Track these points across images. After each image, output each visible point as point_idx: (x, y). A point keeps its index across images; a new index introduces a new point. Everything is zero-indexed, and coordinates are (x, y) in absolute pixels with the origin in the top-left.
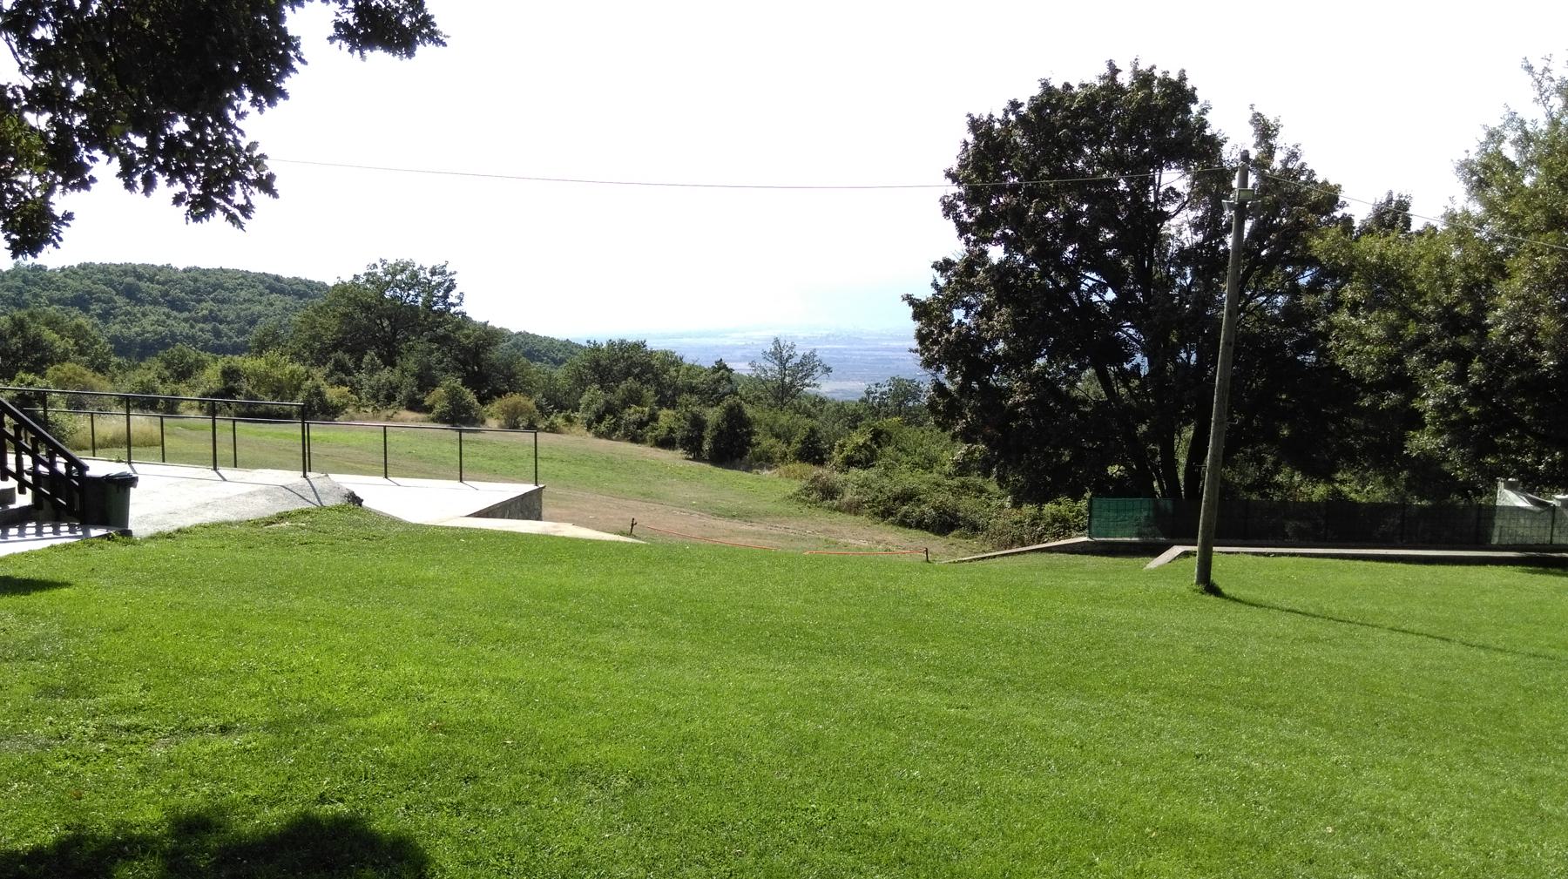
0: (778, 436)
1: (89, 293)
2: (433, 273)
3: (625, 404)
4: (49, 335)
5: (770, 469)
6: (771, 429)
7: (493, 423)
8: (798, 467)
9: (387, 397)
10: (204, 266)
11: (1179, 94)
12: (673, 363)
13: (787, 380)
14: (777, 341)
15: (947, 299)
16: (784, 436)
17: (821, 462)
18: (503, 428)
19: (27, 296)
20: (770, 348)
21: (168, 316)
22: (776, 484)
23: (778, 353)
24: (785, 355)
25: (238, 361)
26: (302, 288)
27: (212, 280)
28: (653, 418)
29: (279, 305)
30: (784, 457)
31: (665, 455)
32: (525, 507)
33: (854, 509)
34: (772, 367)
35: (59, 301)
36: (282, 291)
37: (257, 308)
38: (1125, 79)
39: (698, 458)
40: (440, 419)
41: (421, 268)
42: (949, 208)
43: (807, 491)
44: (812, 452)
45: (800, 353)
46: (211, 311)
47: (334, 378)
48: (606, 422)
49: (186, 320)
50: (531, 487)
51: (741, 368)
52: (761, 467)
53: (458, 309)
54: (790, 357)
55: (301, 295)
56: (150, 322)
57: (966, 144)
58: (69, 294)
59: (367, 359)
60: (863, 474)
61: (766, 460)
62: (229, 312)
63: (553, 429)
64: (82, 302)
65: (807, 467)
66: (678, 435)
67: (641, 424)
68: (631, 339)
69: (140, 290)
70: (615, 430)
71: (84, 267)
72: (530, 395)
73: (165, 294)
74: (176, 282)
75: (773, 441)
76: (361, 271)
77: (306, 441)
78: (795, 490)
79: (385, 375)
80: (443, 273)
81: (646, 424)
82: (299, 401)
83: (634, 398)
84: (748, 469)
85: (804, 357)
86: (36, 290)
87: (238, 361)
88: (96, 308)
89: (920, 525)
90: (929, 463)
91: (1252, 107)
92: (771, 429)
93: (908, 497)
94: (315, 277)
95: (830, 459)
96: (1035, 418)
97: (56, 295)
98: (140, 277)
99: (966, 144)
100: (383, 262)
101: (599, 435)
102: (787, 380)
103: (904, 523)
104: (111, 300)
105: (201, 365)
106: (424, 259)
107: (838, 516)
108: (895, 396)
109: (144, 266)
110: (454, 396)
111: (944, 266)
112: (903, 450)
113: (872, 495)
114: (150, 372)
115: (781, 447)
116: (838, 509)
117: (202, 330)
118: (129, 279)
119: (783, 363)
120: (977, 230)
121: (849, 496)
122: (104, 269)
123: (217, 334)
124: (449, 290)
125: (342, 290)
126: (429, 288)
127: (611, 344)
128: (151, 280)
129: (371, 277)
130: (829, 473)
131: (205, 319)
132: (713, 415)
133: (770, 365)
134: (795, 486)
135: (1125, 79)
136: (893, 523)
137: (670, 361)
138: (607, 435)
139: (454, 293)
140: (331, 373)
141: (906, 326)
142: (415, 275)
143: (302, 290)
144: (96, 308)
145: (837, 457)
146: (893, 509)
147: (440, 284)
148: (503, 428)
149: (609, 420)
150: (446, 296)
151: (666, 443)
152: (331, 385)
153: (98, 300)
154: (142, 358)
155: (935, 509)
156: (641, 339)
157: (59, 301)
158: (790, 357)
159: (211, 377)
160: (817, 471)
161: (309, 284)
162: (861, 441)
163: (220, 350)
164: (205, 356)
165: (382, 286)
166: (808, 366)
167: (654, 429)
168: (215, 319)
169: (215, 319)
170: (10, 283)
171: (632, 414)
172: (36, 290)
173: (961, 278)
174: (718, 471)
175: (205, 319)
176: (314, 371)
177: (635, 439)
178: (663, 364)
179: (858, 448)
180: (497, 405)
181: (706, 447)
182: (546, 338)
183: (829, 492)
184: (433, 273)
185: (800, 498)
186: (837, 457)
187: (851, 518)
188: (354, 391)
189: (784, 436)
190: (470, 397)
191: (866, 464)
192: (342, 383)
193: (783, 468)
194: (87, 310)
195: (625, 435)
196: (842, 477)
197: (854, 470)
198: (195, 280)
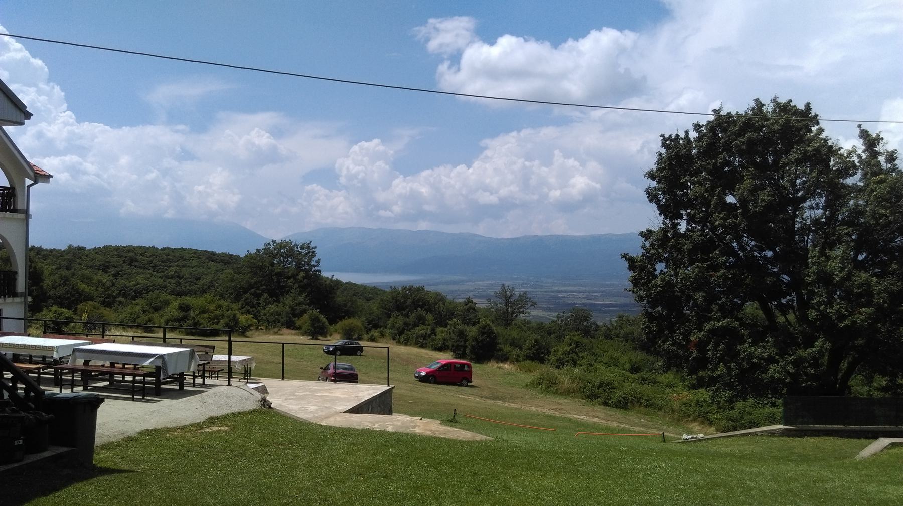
3: (416, 325)
4: (82, 286)
11: (807, 117)
12: (440, 300)
15: (651, 258)
16: (514, 344)
21: (152, 275)
25: (188, 300)
27: (177, 254)
28: (433, 332)
29: (213, 269)
32: (380, 405)
33: (568, 393)
37: (201, 270)
38: (769, 108)
41: (296, 245)
42: (652, 196)
44: (538, 355)
45: (517, 294)
46: (176, 272)
47: (244, 310)
48: (788, 436)
49: (161, 278)
50: (385, 388)
51: (481, 304)
53: (316, 268)
54: (511, 296)
55: (226, 263)
56: (141, 279)
57: (660, 155)
61: (504, 359)
62: (186, 272)
63: (372, 339)
66: (450, 343)
67: (425, 337)
71: (105, 247)
77: (230, 342)
79: (272, 308)
81: (429, 336)
83: (421, 321)
87: (188, 300)
88: (113, 271)
90: (615, 362)
91: (860, 126)
94: (234, 252)
98: (136, 254)
99: (660, 155)
105: (167, 303)
109: (139, 247)
111: (647, 235)
114: (137, 306)
117: (169, 283)
118: (131, 254)
120: (669, 210)
122: (117, 248)
123: (179, 284)
125: (250, 258)
127: (404, 289)
129: (267, 250)
131: (172, 277)
132: (472, 332)
134: (529, 378)
135: (769, 108)
137: (440, 299)
139: (314, 259)
140: (242, 307)
141: (624, 276)
142: (292, 249)
143: (227, 260)
146: (597, 394)
150: (310, 261)
152: (242, 314)
154: (134, 298)
156: (421, 285)
157: (91, 267)
158: (511, 296)
159: (172, 310)
162: (569, 348)
163: (179, 294)
164: (169, 297)
166: (524, 301)
168: (179, 277)
169: (179, 277)
170: (66, 257)
173: (661, 243)
175: (172, 277)
176: (233, 306)
180: (341, 324)
182: (362, 286)
184: (302, 248)
186: (553, 358)
188: (255, 317)
190: (323, 318)
192: (248, 312)
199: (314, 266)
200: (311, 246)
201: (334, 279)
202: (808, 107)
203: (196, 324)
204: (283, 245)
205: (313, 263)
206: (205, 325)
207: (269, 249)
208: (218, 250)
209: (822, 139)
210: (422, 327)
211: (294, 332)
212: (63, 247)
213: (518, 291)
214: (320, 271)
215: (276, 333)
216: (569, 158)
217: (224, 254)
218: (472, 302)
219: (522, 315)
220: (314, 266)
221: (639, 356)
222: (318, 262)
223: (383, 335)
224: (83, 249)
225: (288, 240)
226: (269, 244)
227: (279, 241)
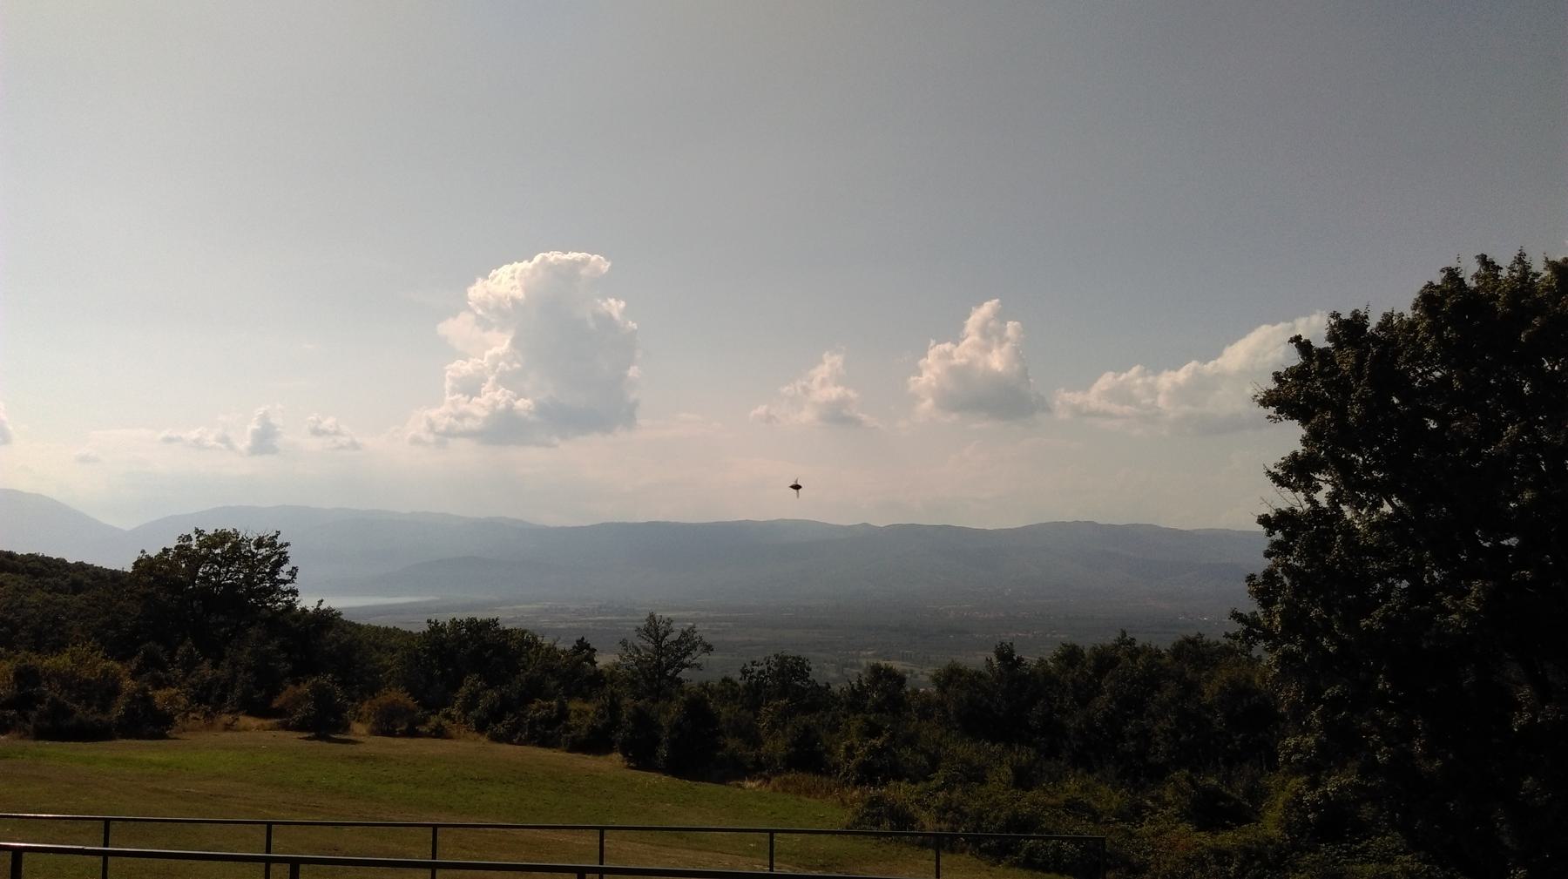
3: (526, 699)
7: (359, 729)
9: (210, 700)
14: (652, 616)
23: (654, 629)
24: (661, 633)
26: (38, 565)
33: (940, 844)
36: (15, 570)
59: (182, 650)
67: (549, 722)
76: (172, 544)
80: (272, 544)
82: (118, 709)
85: (684, 634)
93: (1023, 825)
96: (672, 678)
100: (199, 532)
101: (496, 738)
124: (279, 564)
126: (250, 561)
129: (182, 550)
130: (900, 792)
132: (669, 714)
133: (644, 643)
138: (506, 739)
139: (286, 568)
142: (236, 546)
147: (269, 557)
149: (509, 719)
150: (274, 572)
151: (595, 744)
158: (667, 633)
161: (47, 562)
166: (688, 643)
177: (545, 742)
183: (902, 821)
199: (285, 582)
200: (279, 541)
201: (322, 607)
204: (221, 538)
205: (282, 576)
207: (188, 548)
208: (21, 549)
209: (1381, 327)
211: (268, 722)
214: (295, 593)
215: (228, 727)
216: (196, 441)
217: (32, 558)
218: (587, 647)
219: (685, 670)
220: (285, 582)
222: (293, 573)
224: (63, 562)
225: (250, 529)
226: (189, 538)
227: (210, 532)
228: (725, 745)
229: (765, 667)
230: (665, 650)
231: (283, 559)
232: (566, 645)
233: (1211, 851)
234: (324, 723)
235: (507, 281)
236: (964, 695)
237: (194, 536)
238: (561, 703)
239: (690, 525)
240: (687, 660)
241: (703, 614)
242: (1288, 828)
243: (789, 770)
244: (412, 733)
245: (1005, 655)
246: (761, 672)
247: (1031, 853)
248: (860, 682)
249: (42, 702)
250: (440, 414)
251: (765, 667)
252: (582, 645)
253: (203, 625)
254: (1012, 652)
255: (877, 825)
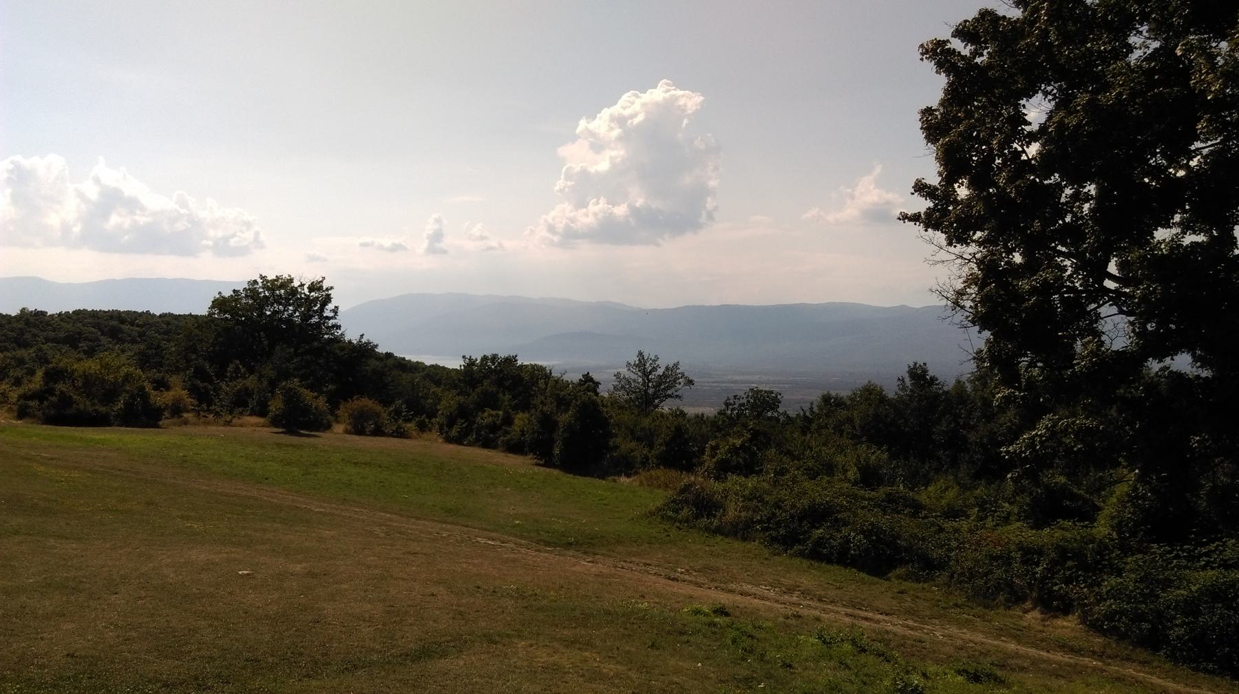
0: (639, 439)
1: (80, 333)
2: (311, 289)
3: (480, 407)
5: (628, 476)
6: (632, 432)
8: (661, 473)
10: (176, 312)
13: (651, 391)
17: (689, 468)
18: (347, 432)
19: (27, 336)
20: (634, 359)
22: (635, 495)
28: (508, 421)
30: (645, 463)
31: (498, 458)
33: (741, 531)
34: (635, 376)
35: (54, 340)
39: (548, 464)
40: (275, 422)
43: (675, 505)
52: (619, 474)
53: (331, 322)
58: (62, 335)
59: (231, 368)
60: (751, 482)
61: (626, 466)
64: (72, 341)
65: (673, 474)
67: (494, 428)
68: (503, 354)
69: (121, 331)
70: (467, 435)
71: (77, 313)
72: (386, 403)
73: (141, 335)
74: (151, 325)
75: (633, 444)
78: (659, 503)
80: (320, 289)
81: (499, 428)
84: (602, 476)
86: (35, 331)
89: (843, 558)
92: (632, 432)
93: (818, 515)
95: (701, 464)
97: (52, 334)
101: (449, 440)
102: (651, 391)
103: (818, 554)
104: (97, 339)
106: (302, 274)
107: (720, 543)
108: (753, 407)
109: (128, 313)
110: (292, 399)
112: (789, 453)
113: (766, 512)
115: (640, 451)
116: (718, 531)
118: (114, 323)
119: (646, 374)
121: (733, 511)
122: (94, 314)
128: (132, 324)
134: (658, 498)
136: (801, 554)
138: (458, 441)
139: (330, 306)
142: (294, 291)
144: (83, 345)
145: (709, 462)
148: (347, 432)
150: (322, 309)
151: (515, 448)
152: (127, 378)
153: (86, 339)
155: (867, 534)
157: (54, 340)
158: (654, 369)
160: (687, 479)
162: (738, 442)
165: (261, 303)
167: (507, 433)
171: (486, 417)
172: (35, 331)
174: (567, 478)
177: (487, 444)
178: (532, 378)
179: (735, 450)
181: (557, 451)
183: (705, 506)
185: (663, 515)
186: (709, 462)
187: (737, 544)
189: (647, 438)
191: (749, 468)
193: (644, 474)
194: (76, 348)
195: (477, 440)
196: (717, 486)
197: (733, 478)
198: (168, 324)
199: (328, 318)
200: (325, 285)
201: (363, 340)
202: (938, 53)
203: (66, 401)
205: (327, 313)
206: (84, 404)
210: (488, 411)
212: (14, 311)
213: (664, 362)
215: (228, 423)
218: (591, 380)
221: (878, 456)
222: (335, 311)
223: (422, 427)
224: (43, 313)
226: (255, 282)
227: (271, 277)
228: (617, 447)
229: (745, 401)
230: (653, 385)
231: (328, 299)
232: (575, 377)
233: (1020, 547)
234: (297, 421)
235: (635, 105)
236: (871, 411)
237: (260, 281)
238: (506, 412)
239: (752, 307)
240: (669, 392)
241: (765, 378)
242: (1119, 527)
243: (658, 466)
244: (378, 432)
245: (919, 375)
246: (740, 405)
247: (820, 543)
248: (811, 409)
249: (53, 395)
250: (561, 213)
251: (745, 401)
252: (587, 378)
253: (272, 354)
254: (925, 371)
255: (677, 511)
